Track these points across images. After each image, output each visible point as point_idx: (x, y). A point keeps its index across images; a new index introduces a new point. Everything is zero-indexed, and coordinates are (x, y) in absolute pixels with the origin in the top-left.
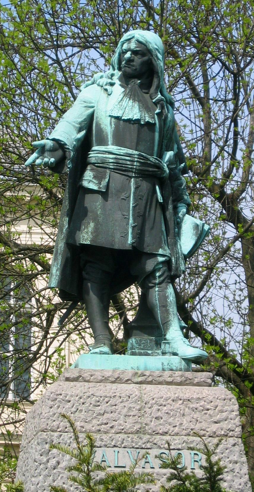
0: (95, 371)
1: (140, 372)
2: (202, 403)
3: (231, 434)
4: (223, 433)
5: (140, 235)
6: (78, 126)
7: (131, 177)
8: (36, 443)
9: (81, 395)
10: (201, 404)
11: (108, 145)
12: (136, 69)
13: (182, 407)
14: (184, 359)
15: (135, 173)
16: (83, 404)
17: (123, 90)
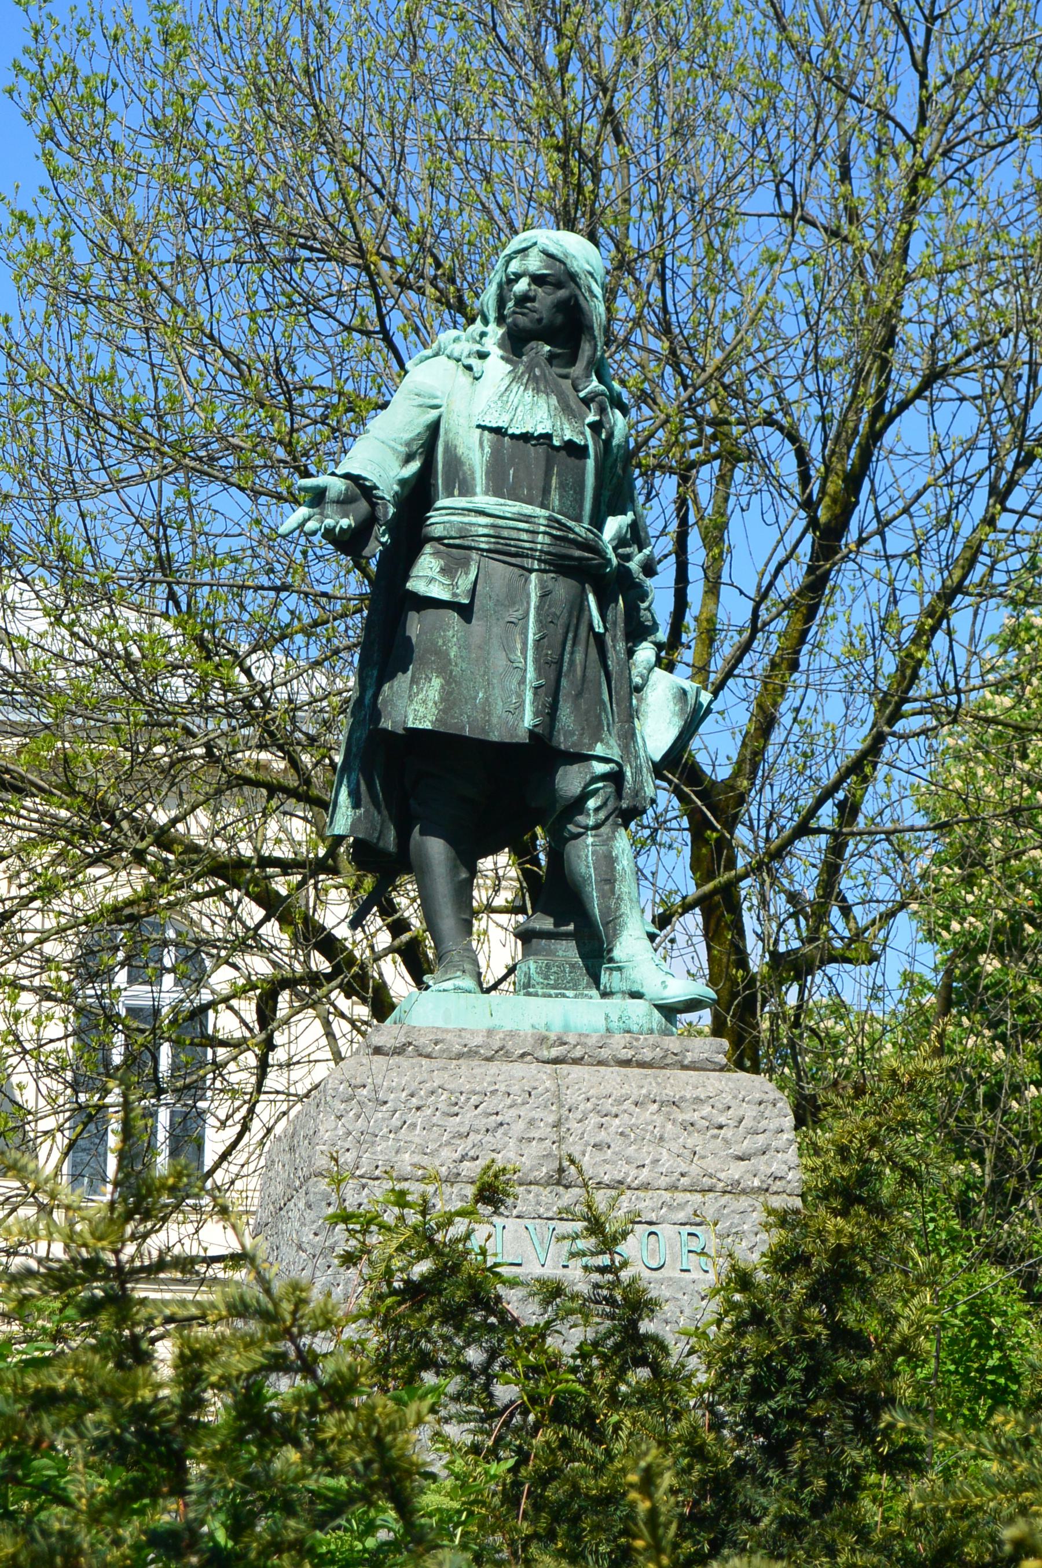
0: (446, 1031)
1: (553, 1037)
2: (706, 1110)
3: (778, 1186)
4: (757, 1183)
5: (550, 712)
6: (403, 449)
7: (531, 571)
8: (301, 1205)
9: (415, 1085)
10: (704, 1113)
11: (474, 494)
12: (540, 320)
13: (659, 1119)
14: (659, 1007)
15: (540, 560)
16: (418, 1109)
17: (509, 367)
